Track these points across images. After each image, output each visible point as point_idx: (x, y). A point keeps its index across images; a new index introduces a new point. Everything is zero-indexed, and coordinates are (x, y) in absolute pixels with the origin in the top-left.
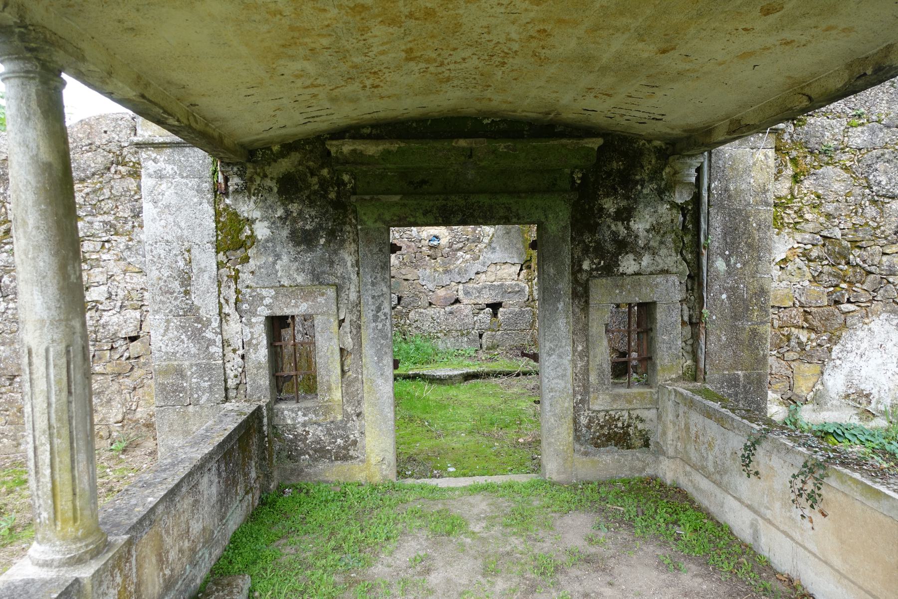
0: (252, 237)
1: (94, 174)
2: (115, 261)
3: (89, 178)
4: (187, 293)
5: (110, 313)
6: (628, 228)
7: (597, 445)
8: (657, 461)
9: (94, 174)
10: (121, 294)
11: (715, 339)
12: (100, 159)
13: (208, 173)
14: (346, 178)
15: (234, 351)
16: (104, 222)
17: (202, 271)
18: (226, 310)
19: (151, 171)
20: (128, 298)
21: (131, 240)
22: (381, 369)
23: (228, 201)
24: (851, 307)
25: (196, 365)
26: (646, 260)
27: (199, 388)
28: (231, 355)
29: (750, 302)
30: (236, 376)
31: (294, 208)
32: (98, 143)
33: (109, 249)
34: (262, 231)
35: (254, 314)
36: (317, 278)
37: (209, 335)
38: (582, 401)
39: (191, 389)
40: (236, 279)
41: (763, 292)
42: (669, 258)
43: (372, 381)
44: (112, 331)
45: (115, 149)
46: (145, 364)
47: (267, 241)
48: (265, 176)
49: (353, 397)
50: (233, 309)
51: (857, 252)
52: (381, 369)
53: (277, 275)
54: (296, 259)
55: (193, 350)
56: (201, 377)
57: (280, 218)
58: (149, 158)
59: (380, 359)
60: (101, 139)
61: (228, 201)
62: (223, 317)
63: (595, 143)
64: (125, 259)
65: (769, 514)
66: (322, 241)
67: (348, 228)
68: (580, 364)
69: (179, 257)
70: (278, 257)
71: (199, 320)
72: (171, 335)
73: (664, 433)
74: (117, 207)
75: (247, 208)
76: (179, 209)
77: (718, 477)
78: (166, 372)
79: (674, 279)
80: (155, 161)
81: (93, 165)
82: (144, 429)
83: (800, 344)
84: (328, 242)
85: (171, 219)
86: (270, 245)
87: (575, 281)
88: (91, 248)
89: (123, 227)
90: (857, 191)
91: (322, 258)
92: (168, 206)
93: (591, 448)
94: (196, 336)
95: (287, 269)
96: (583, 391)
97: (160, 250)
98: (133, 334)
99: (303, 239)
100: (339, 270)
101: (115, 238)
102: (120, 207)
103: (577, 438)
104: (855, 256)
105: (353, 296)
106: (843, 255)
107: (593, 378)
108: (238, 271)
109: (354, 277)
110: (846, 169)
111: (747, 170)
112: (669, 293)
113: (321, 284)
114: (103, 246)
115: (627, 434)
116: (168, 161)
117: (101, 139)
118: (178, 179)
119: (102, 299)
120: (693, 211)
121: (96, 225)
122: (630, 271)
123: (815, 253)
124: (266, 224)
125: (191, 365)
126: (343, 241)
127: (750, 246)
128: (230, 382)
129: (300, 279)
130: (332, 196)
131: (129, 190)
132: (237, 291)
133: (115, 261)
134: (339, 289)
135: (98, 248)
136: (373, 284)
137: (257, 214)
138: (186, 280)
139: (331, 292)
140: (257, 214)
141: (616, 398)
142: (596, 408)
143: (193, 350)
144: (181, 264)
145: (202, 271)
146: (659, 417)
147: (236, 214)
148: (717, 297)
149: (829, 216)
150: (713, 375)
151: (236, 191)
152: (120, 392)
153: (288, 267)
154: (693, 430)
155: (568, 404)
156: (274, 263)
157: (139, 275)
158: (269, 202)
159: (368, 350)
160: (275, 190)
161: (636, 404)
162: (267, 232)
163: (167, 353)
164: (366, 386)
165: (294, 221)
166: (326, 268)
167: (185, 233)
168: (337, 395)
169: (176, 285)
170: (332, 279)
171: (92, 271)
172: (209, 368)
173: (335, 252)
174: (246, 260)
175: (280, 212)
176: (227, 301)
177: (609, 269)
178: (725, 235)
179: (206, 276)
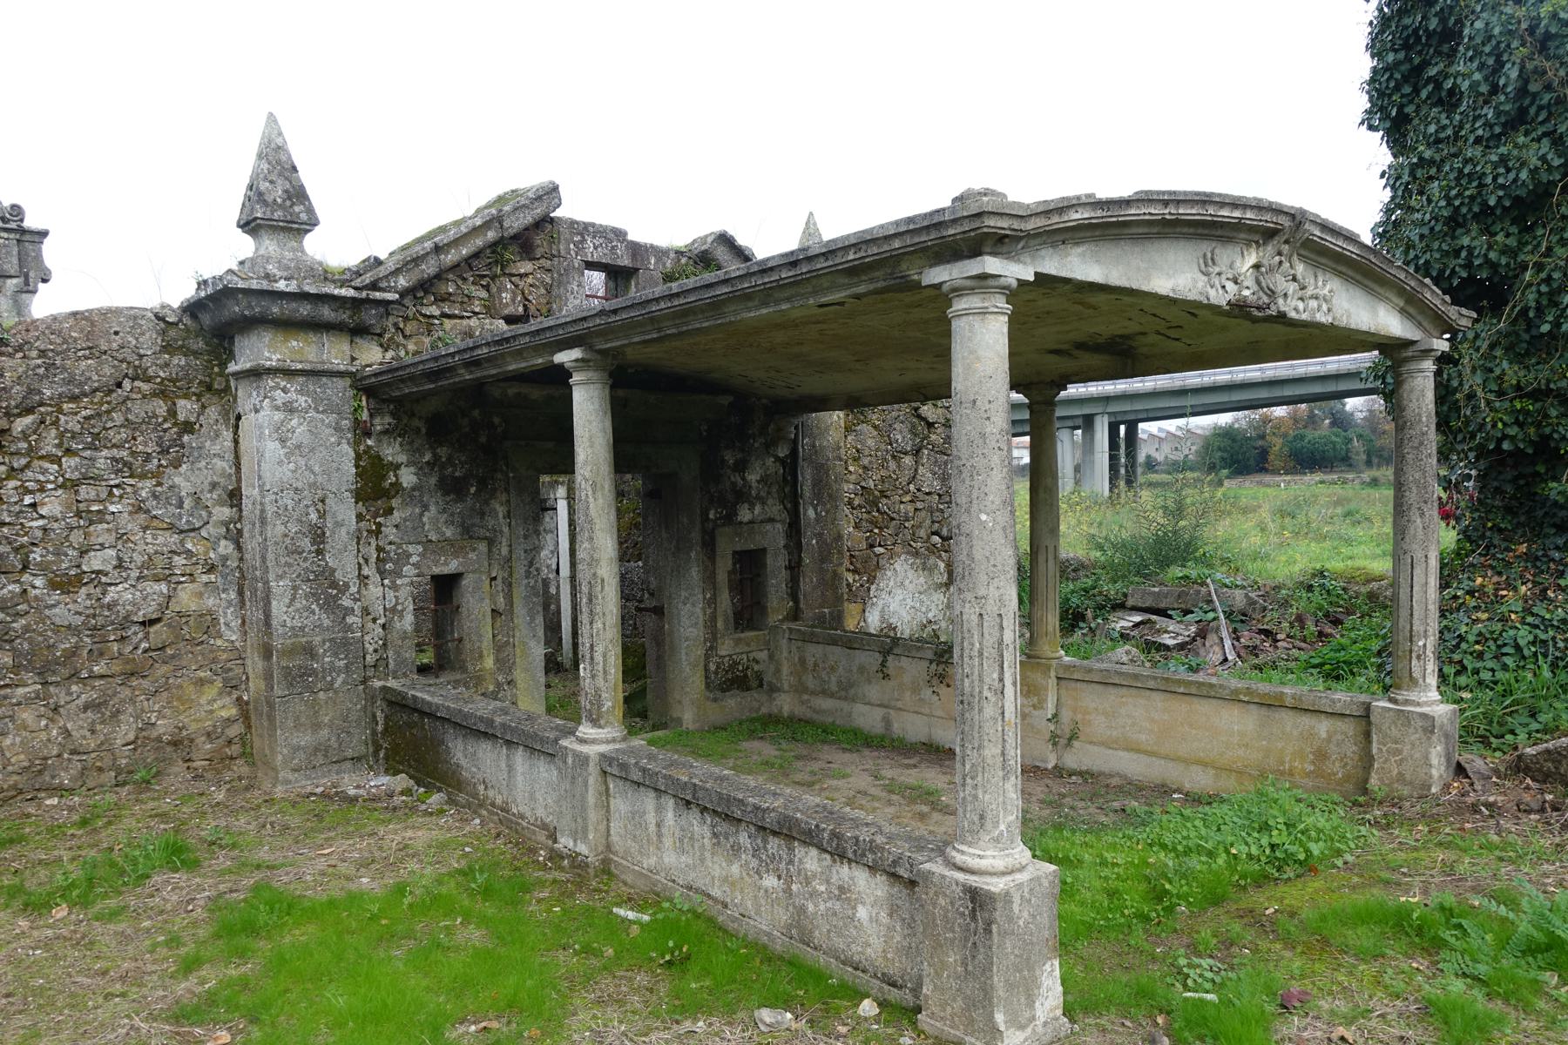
0: (396, 485)
1: (95, 391)
2: (130, 513)
3: (86, 395)
4: (319, 552)
5: (120, 587)
6: (744, 479)
7: (724, 691)
8: (772, 699)
9: (95, 391)
10: (139, 559)
11: (808, 583)
12: (107, 370)
13: (347, 409)
14: (496, 420)
15: (374, 620)
16: (113, 459)
17: (338, 524)
18: (366, 571)
19: (279, 402)
20: (149, 563)
21: (159, 484)
22: (534, 629)
23: (369, 442)
24: (881, 550)
25: (330, 640)
26: (758, 509)
27: (333, 669)
28: (370, 625)
29: (830, 546)
30: (376, 651)
31: (443, 452)
32: (104, 348)
33: (121, 497)
34: (408, 478)
35: (400, 576)
36: (467, 532)
37: (346, 602)
38: (711, 648)
39: (324, 670)
40: (378, 533)
41: (839, 537)
42: (775, 508)
43: (525, 644)
44: (123, 613)
45: (132, 358)
46: (173, 657)
47: (413, 489)
48: (413, 415)
49: (505, 664)
50: (374, 570)
51: (885, 501)
52: (534, 629)
53: (423, 531)
54: (444, 510)
55: (326, 622)
56: (336, 655)
57: (428, 463)
58: (277, 387)
59: (533, 619)
60: (109, 342)
61: (369, 442)
62: (363, 579)
63: (725, 400)
64: (147, 511)
65: (899, 704)
66: (473, 490)
67: (499, 476)
68: (709, 611)
69: (312, 509)
70: (425, 508)
71: (334, 585)
72: (298, 605)
73: (778, 671)
74: (134, 439)
75: (392, 452)
76: (312, 450)
77: (843, 693)
78: (291, 652)
79: (779, 526)
80: (285, 390)
81: (95, 378)
82: (169, 749)
83: (848, 585)
84: (478, 491)
85: (302, 462)
86: (416, 493)
87: (704, 531)
88: (92, 495)
89: (142, 466)
90: (883, 447)
91: (473, 509)
92: (299, 447)
93: (719, 694)
94: (331, 605)
95: (435, 521)
96: (713, 637)
97: (288, 500)
98: (154, 616)
99: (452, 488)
100: (491, 523)
101: (131, 481)
102: (140, 439)
103: (708, 686)
104: (883, 504)
105: (505, 551)
106: (874, 503)
107: (720, 624)
108: (379, 525)
109: (506, 530)
110: (875, 427)
111: (827, 429)
112: (774, 538)
113: (471, 538)
114: (111, 494)
115: (746, 676)
116: (301, 392)
117: (109, 342)
118: (312, 413)
119: (109, 568)
120: (791, 465)
121: (101, 463)
122: (746, 519)
123: (856, 503)
124: (412, 469)
125: (324, 642)
126: (495, 490)
127: (830, 496)
128: (368, 657)
129: (449, 533)
130: (483, 439)
131: (156, 417)
132: (379, 549)
133: (130, 513)
134: (491, 542)
135: (104, 496)
136: (526, 537)
137: (402, 458)
138: (319, 537)
139: (483, 547)
140: (402, 458)
141: (738, 642)
142: (723, 653)
143: (326, 622)
144: (314, 516)
145: (338, 524)
146: (771, 657)
147: (379, 457)
148: (810, 541)
149: (865, 468)
150: (808, 614)
151: (385, 432)
152: (132, 701)
153: (436, 520)
154: (810, 661)
155: (700, 652)
156: (421, 515)
157: (167, 534)
158: (416, 445)
159: (520, 610)
160: (424, 430)
161: (754, 646)
162: (414, 479)
163: (293, 628)
164: (518, 651)
165: (443, 467)
166: (477, 520)
167: (320, 479)
168: (489, 662)
169: (306, 543)
170: (482, 532)
171: (92, 528)
172: (345, 643)
173: (487, 503)
174: (389, 511)
175: (428, 457)
176: (366, 561)
177: (730, 518)
178: (814, 486)
179: (343, 531)
